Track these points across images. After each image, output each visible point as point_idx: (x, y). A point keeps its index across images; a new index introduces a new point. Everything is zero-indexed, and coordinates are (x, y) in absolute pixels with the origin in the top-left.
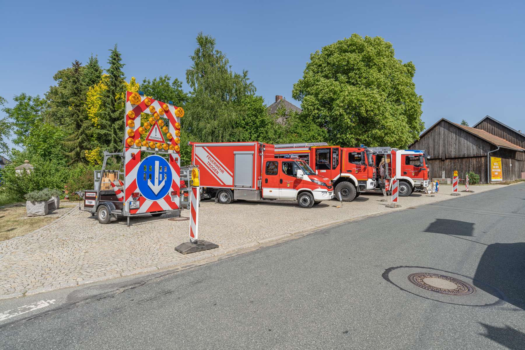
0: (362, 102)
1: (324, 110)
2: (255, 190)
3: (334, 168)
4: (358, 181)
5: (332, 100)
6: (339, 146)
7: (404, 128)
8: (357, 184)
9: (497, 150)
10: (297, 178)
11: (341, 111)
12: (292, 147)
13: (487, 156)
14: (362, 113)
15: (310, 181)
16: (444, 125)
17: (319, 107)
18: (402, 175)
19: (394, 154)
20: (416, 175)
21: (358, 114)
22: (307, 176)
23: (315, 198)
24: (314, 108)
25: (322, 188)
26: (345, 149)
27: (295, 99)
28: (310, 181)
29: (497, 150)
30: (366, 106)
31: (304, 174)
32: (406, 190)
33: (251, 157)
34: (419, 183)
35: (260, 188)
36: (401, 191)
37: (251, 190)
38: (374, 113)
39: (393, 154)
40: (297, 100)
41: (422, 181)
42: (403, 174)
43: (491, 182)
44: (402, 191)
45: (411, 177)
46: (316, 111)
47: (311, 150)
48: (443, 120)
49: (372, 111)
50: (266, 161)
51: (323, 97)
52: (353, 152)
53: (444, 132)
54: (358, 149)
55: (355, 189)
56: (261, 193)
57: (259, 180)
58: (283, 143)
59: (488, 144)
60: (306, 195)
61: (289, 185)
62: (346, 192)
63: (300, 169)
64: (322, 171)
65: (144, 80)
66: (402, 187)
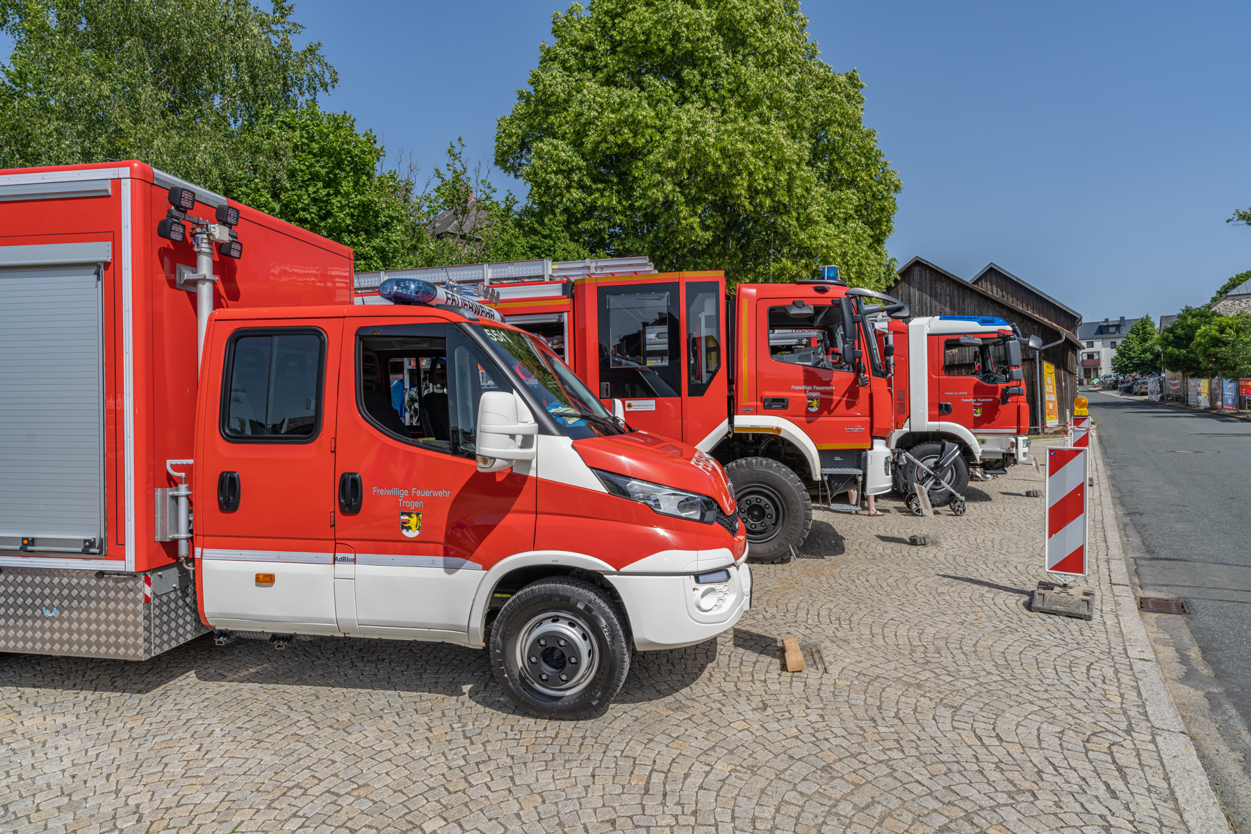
1: (604, 189)
2: (133, 576)
4: (820, 452)
5: (635, 154)
6: (722, 273)
7: (864, 262)
8: (817, 472)
9: (1060, 342)
10: (481, 467)
13: (1033, 360)
14: (739, 196)
15: (594, 483)
16: (921, 276)
17: (588, 181)
18: (931, 419)
19: (902, 334)
20: (985, 419)
21: (724, 205)
22: (567, 442)
23: (637, 634)
24: (571, 181)
27: (506, 170)
28: (594, 483)
29: (1060, 342)
30: (751, 174)
31: (543, 430)
33: (89, 288)
34: (998, 449)
35: (183, 550)
37: (100, 574)
38: (773, 200)
39: (895, 333)
40: (512, 174)
41: (1014, 440)
42: (936, 412)
45: (976, 424)
46: (576, 194)
48: (918, 263)
49: (770, 193)
50: (229, 329)
51: (601, 142)
53: (921, 300)
54: (817, 290)
56: (190, 585)
57: (172, 482)
59: (1036, 327)
60: (562, 605)
61: (413, 521)
62: (762, 514)
63: (505, 386)
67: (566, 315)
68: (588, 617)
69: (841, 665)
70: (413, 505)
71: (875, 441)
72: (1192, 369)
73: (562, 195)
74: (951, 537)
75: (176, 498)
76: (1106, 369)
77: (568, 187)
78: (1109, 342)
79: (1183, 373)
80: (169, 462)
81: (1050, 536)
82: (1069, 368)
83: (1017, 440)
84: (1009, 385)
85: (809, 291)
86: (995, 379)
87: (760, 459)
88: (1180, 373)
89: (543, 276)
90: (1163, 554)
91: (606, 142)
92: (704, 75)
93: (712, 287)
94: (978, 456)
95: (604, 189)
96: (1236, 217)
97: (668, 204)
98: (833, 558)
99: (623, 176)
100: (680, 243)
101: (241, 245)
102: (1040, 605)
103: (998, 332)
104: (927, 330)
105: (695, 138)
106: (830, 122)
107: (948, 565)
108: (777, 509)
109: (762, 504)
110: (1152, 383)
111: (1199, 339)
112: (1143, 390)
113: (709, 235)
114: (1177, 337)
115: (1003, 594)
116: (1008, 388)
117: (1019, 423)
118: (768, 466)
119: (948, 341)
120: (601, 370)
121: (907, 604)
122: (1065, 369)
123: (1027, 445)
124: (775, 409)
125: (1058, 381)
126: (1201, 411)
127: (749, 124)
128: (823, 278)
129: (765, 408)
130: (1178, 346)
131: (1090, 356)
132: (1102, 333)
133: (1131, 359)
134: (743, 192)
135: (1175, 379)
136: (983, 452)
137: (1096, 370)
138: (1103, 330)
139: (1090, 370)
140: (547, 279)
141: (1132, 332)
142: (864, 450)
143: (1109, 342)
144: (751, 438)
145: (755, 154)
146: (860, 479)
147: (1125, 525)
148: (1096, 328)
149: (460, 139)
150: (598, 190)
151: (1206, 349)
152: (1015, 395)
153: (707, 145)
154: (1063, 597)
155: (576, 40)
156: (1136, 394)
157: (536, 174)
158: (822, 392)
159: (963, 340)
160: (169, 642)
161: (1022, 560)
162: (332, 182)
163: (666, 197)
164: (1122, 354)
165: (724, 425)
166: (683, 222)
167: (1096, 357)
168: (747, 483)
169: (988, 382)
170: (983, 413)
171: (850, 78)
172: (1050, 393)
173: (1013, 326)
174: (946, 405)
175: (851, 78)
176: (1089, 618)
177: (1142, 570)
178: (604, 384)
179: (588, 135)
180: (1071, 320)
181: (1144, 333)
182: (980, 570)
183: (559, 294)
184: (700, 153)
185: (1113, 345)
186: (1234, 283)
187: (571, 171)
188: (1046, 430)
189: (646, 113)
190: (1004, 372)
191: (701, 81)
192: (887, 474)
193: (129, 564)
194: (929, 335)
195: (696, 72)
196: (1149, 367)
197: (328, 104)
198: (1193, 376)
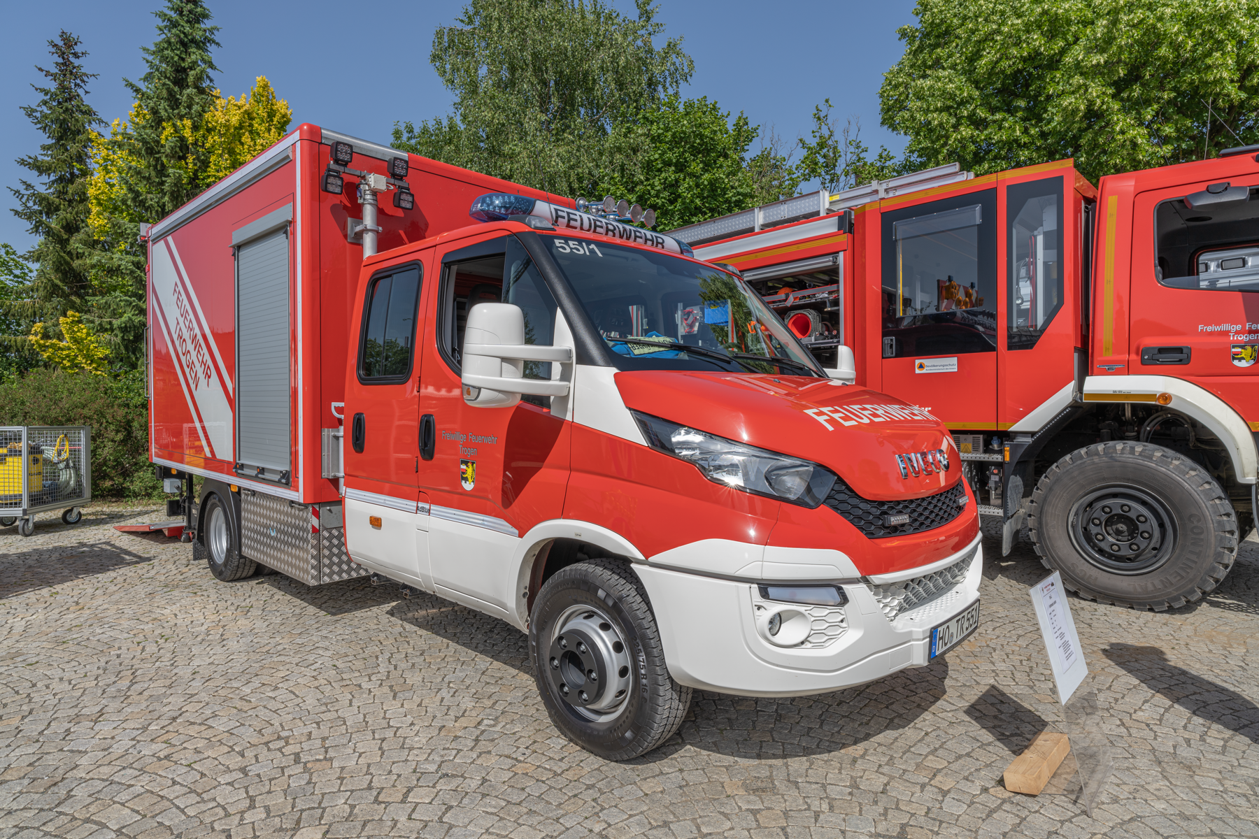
0: (1215, 28)
11: (1095, 90)
12: (750, 231)
17: (981, 113)
25: (773, 537)
46: (966, 131)
52: (990, 748)
55: (1226, 506)
61: (470, 471)
64: (926, 362)
65: (392, 131)
67: (841, 255)
68: (616, 614)
69: (1135, 809)
70: (471, 452)
73: (947, 137)
75: (337, 438)
77: (956, 127)
80: (334, 404)
89: (818, 213)
93: (1053, 186)
97: (1094, 115)
101: (412, 195)
109: (1133, 515)
120: (885, 321)
124: (1163, 363)
129: (1143, 363)
140: (822, 214)
144: (1128, 413)
149: (827, 101)
153: (1160, 19)
160: (339, 574)
162: (681, 167)
163: (1091, 103)
168: (1128, 480)
178: (887, 340)
179: (982, 56)
183: (835, 230)
184: (1152, 39)
187: (963, 103)
193: (298, 496)
197: (688, 93)
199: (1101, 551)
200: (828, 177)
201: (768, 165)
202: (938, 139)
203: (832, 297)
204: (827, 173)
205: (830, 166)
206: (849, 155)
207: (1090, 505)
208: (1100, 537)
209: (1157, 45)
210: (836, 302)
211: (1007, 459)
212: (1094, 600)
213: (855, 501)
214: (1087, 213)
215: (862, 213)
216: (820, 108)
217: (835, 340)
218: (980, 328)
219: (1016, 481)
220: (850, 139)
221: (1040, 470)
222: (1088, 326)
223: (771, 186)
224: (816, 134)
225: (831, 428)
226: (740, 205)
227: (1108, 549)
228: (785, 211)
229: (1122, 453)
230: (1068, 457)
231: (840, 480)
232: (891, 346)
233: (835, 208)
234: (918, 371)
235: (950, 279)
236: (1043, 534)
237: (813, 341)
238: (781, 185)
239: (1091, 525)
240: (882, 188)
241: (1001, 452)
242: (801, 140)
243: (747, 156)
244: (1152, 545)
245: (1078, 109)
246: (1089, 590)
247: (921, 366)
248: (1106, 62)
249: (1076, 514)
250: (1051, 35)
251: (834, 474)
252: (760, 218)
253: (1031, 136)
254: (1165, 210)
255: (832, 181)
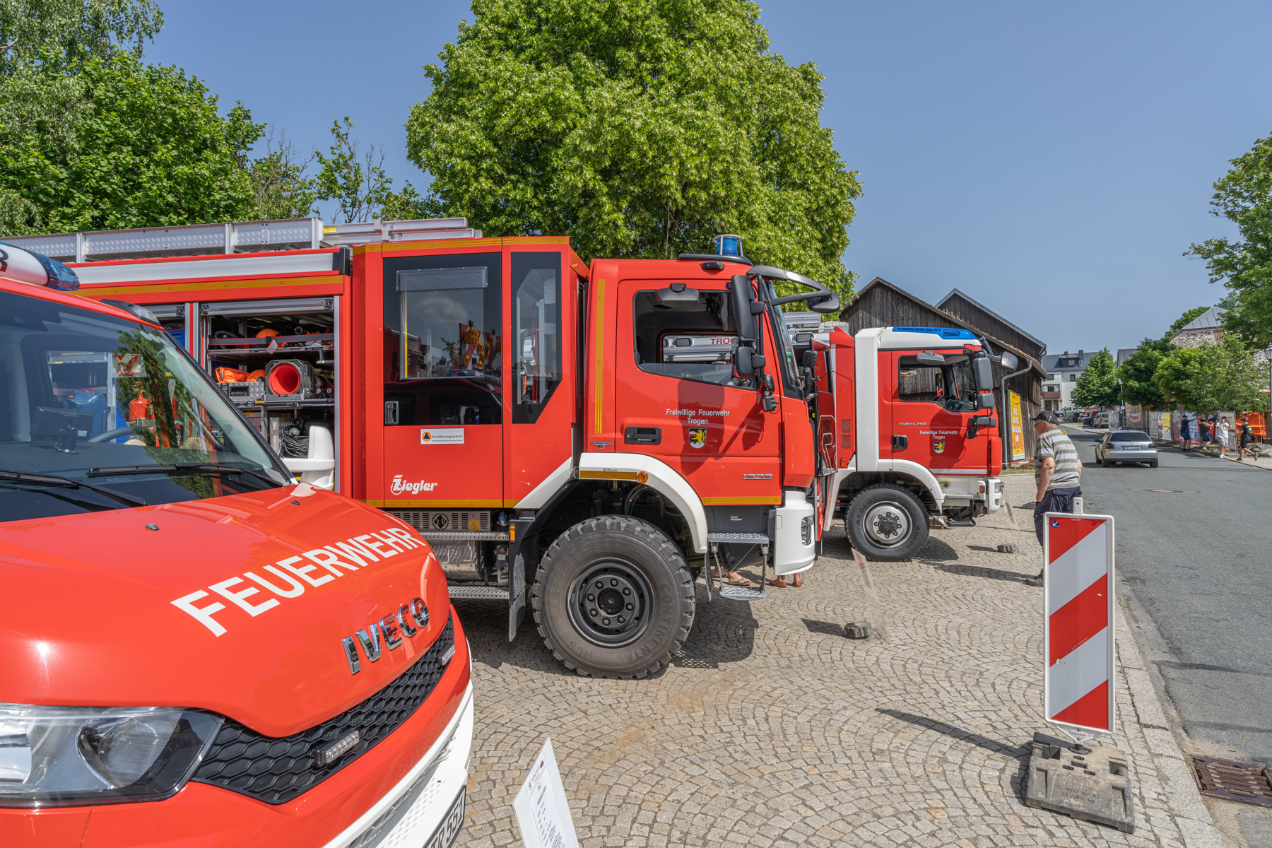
1: (518, 181)
3: (526, 414)
4: (708, 510)
6: (565, 240)
8: (702, 537)
9: (1026, 370)
12: (217, 252)
14: (668, 187)
16: (882, 298)
18: (883, 455)
19: (847, 348)
21: (652, 201)
26: (608, 270)
29: (1026, 370)
32: (902, 520)
36: (882, 536)
38: (709, 195)
39: (838, 347)
42: (889, 448)
43: (1012, 465)
44: (887, 533)
46: (486, 184)
47: (348, 272)
49: (705, 186)
54: (705, 268)
58: (151, 217)
64: (433, 432)
66: (889, 514)
67: (337, 299)
71: (788, 493)
72: (1151, 401)
73: (468, 184)
74: (903, 620)
76: (1066, 402)
78: (1068, 375)
79: (1143, 406)
81: (1052, 662)
82: (1034, 399)
83: (987, 483)
84: (977, 413)
85: (695, 269)
86: (961, 406)
87: (618, 519)
88: (1140, 406)
89: (309, 244)
90: (1196, 656)
91: (522, 125)
92: (642, 58)
93: (551, 261)
94: (940, 504)
95: (518, 181)
96: (1192, 251)
98: (731, 665)
99: (542, 164)
100: (601, 242)
102: (1041, 796)
103: (963, 348)
104: (878, 344)
105: (618, 119)
106: (782, 119)
107: (895, 681)
108: (641, 596)
109: (619, 588)
110: (1112, 416)
111: (1160, 371)
112: (1103, 423)
113: (633, 234)
114: (1138, 370)
115: (979, 754)
116: (976, 417)
117: (989, 461)
118: (629, 530)
119: (902, 358)
121: (817, 789)
122: (1031, 401)
123: (1000, 490)
124: (641, 443)
125: (1024, 412)
126: (1164, 445)
127: (683, 107)
128: (718, 253)
130: (1138, 379)
131: (1051, 389)
132: (1061, 366)
133: (1090, 391)
134: (672, 183)
135: (1135, 412)
136: (947, 498)
137: (1056, 402)
138: (1063, 363)
139: (1050, 402)
140: (315, 246)
141: (1091, 365)
142: (772, 507)
143: (1068, 375)
144: (615, 486)
145: (688, 141)
146: (765, 550)
147: (1128, 599)
148: (1056, 360)
149: (347, 119)
150: (512, 181)
151: (1169, 381)
152: (984, 426)
154: (1079, 779)
155: (497, 17)
156: (1096, 427)
157: (438, 160)
158: (711, 419)
159: (922, 356)
161: (1002, 670)
164: (1082, 386)
165: (568, 463)
166: (605, 217)
167: (1056, 390)
168: (615, 555)
169: (952, 410)
170: (946, 449)
171: (805, 73)
172: (1016, 425)
173: (981, 341)
174: (901, 439)
175: (806, 75)
176: (1128, 829)
177: (1179, 690)
178: (390, 404)
179: (500, 117)
180: (1036, 348)
181: (1103, 366)
182: (942, 693)
183: (329, 268)
184: (625, 142)
185: (1073, 378)
186: (1187, 319)
187: (481, 157)
188: (1012, 465)
189: (569, 94)
190: (971, 398)
191: (638, 65)
192: (808, 542)
194: (879, 350)
195: (631, 54)
196: (1110, 399)
197: (156, 55)
198: (1153, 409)
199: (594, 626)
200: (349, 200)
201: (275, 172)
202: (460, 184)
203: (326, 348)
204: (348, 195)
205: (352, 189)
206: (372, 183)
207: (586, 581)
208: (594, 613)
209: (629, 149)
210: (330, 355)
211: (513, 538)
212: (589, 676)
213: (262, 747)
214: (581, 291)
215: (361, 255)
216: (338, 123)
217: (330, 400)
218: (492, 388)
219: (519, 560)
220: (373, 165)
221: (545, 543)
222: (582, 400)
223: (279, 197)
224: (335, 151)
225: (218, 630)
226: (231, 211)
227: (600, 624)
228: (267, 235)
229: (611, 529)
230: (566, 534)
231: (230, 722)
232: (394, 411)
233: (331, 243)
234: (423, 442)
235: (471, 324)
236: (545, 615)
237: (303, 399)
238: (292, 198)
239: (587, 602)
240: (386, 230)
241: (506, 529)
242: (318, 154)
243: (251, 156)
244: (635, 615)
245: (576, 187)
246: (585, 667)
247: (427, 437)
248: (596, 151)
249: (574, 591)
250: (555, 117)
251: (220, 716)
252: (232, 238)
253: (540, 201)
254: (641, 298)
255: (353, 205)
